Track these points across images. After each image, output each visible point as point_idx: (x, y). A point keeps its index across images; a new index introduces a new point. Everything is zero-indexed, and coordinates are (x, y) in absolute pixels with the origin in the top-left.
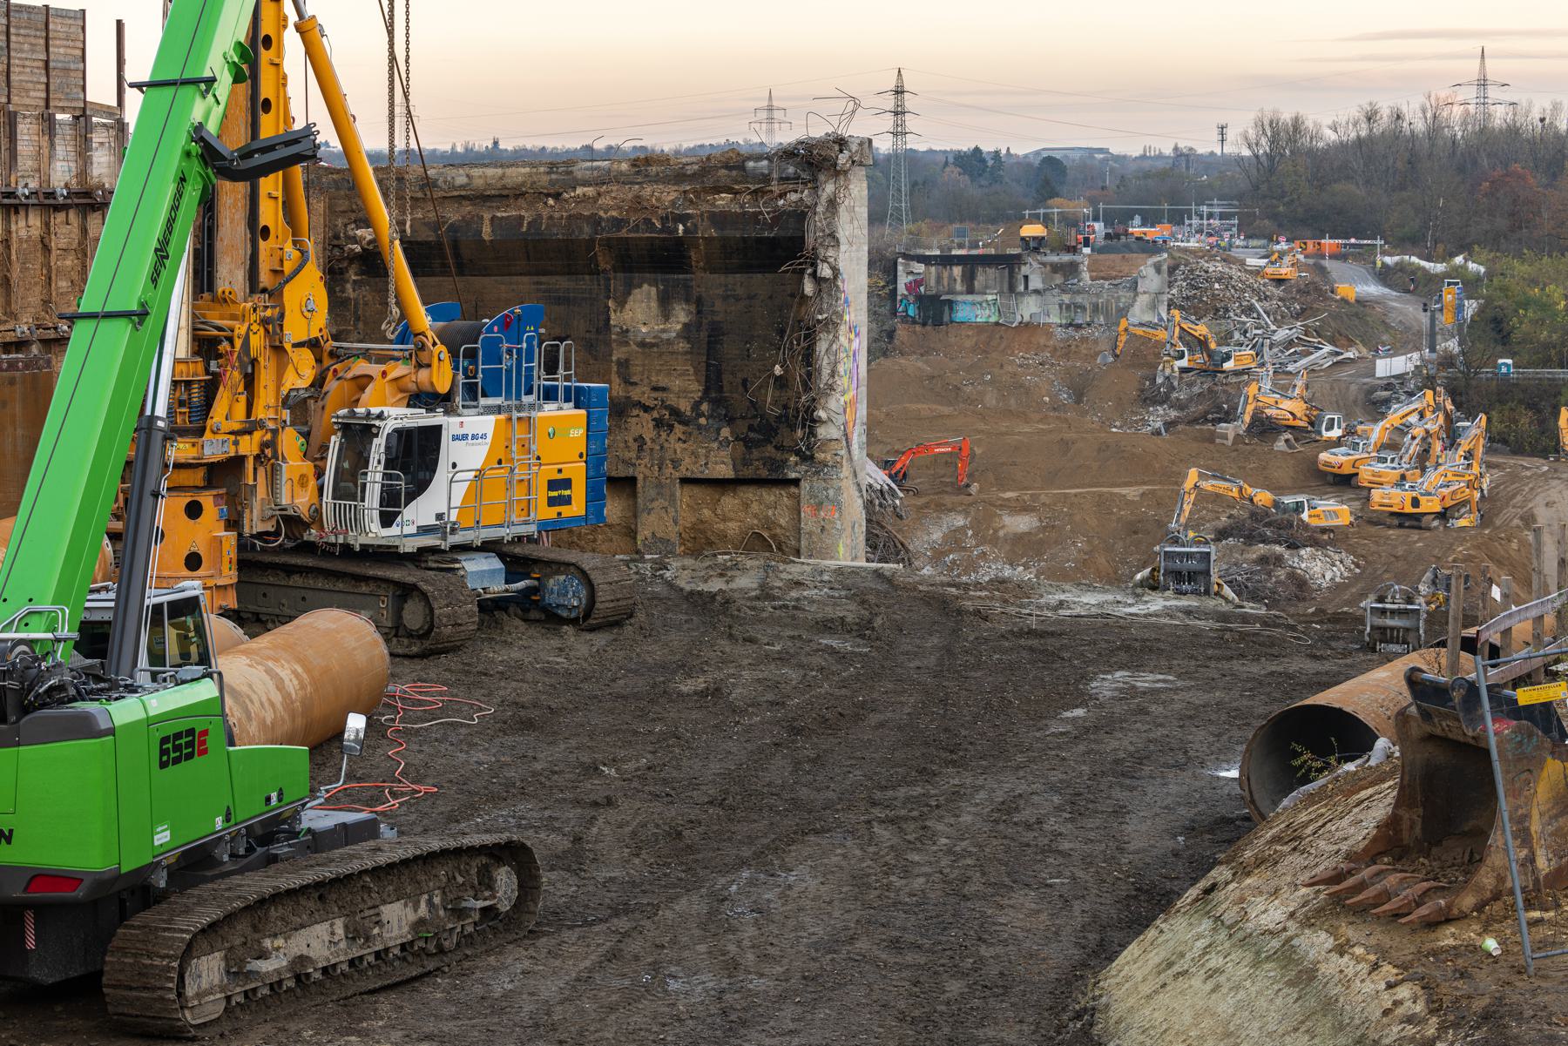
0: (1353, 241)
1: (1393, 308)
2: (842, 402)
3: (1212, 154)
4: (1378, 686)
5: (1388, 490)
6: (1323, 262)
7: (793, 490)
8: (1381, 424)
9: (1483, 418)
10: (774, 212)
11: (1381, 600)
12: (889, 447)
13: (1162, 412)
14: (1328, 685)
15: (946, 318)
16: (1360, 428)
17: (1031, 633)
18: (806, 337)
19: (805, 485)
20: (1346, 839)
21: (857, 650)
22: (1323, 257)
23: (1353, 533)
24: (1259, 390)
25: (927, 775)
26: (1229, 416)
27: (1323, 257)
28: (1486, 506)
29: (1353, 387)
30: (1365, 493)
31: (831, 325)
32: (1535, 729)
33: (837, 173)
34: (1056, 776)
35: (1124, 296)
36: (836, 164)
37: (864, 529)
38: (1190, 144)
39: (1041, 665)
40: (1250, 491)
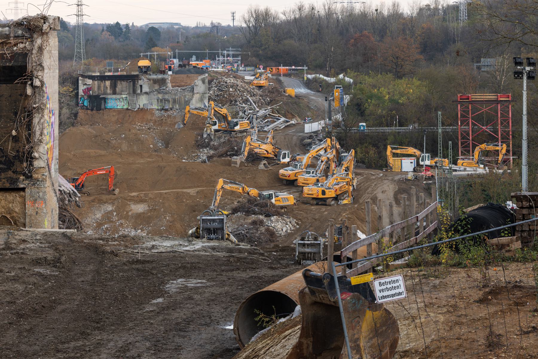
0: (293, 67)
1: (313, 99)
2: (46, 149)
3: (229, 26)
4: (297, 280)
5: (311, 187)
6: (280, 78)
7: (22, 193)
8: (307, 155)
9: (353, 151)
10: (12, 53)
11: (303, 239)
12: (75, 172)
13: (206, 151)
14: (274, 281)
15: (103, 107)
16: (298, 157)
17: (138, 262)
18: (28, 116)
19: (27, 190)
20: (278, 355)
21: (52, 273)
22: (280, 75)
23: (296, 208)
24: (251, 140)
25: (84, 335)
26: (237, 153)
27: (280, 75)
28: (355, 193)
29: (295, 138)
30: (301, 189)
31: (40, 110)
32: (361, 297)
33: (42, 34)
34: (148, 333)
35: (188, 95)
36: (42, 29)
37: (58, 212)
38: (219, 21)
39: (142, 277)
40: (247, 189)
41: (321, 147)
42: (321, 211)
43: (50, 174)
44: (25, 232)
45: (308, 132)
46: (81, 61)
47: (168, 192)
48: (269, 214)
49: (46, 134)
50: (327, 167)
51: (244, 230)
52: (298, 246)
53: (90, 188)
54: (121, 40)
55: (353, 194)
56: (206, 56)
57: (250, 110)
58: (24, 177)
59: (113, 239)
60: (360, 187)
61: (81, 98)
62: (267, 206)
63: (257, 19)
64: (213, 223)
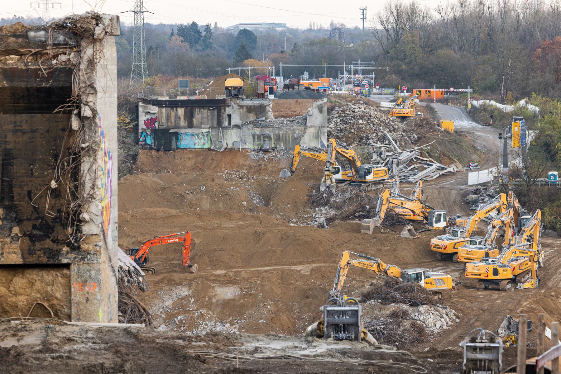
0: (452, 89)
1: (479, 136)
2: (100, 208)
3: (357, 28)
7: (65, 271)
10: (50, 69)
12: (134, 240)
13: (324, 211)
15: (173, 146)
16: (458, 221)
19: (74, 268)
22: (432, 101)
23: (455, 295)
24: (390, 195)
26: (370, 214)
28: (542, 274)
29: (454, 192)
30: (462, 266)
31: (91, 151)
33: (94, 40)
35: (298, 129)
36: (93, 35)
37: (117, 299)
38: (341, 21)
40: (385, 266)
41: (493, 205)
42: (492, 298)
43: (106, 243)
44: (71, 326)
45: (474, 184)
46: (141, 78)
47: (269, 270)
48: (415, 302)
49: (100, 186)
50: (501, 236)
51: (379, 325)
52: (467, 349)
53: (156, 263)
54: (199, 48)
55: (538, 274)
56: (323, 73)
57: (388, 151)
58: (68, 249)
59: (198, 338)
60: (549, 265)
61: (142, 133)
62: (413, 290)
63: (398, 19)
64: (343, 316)
